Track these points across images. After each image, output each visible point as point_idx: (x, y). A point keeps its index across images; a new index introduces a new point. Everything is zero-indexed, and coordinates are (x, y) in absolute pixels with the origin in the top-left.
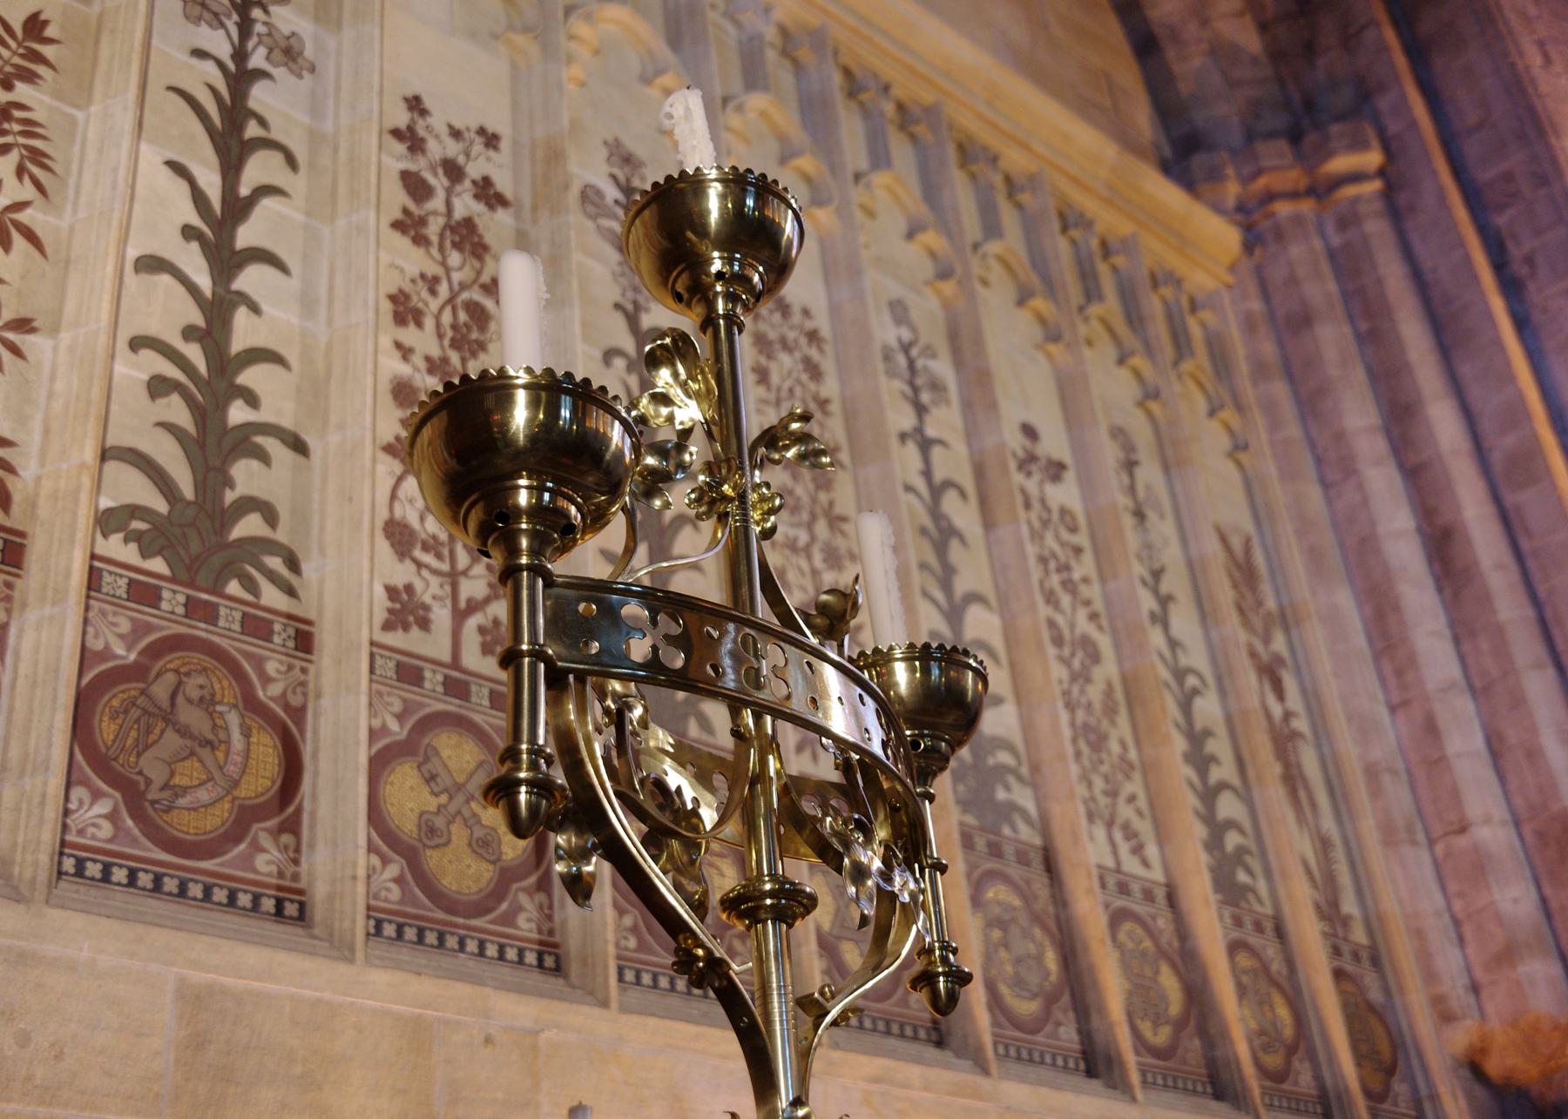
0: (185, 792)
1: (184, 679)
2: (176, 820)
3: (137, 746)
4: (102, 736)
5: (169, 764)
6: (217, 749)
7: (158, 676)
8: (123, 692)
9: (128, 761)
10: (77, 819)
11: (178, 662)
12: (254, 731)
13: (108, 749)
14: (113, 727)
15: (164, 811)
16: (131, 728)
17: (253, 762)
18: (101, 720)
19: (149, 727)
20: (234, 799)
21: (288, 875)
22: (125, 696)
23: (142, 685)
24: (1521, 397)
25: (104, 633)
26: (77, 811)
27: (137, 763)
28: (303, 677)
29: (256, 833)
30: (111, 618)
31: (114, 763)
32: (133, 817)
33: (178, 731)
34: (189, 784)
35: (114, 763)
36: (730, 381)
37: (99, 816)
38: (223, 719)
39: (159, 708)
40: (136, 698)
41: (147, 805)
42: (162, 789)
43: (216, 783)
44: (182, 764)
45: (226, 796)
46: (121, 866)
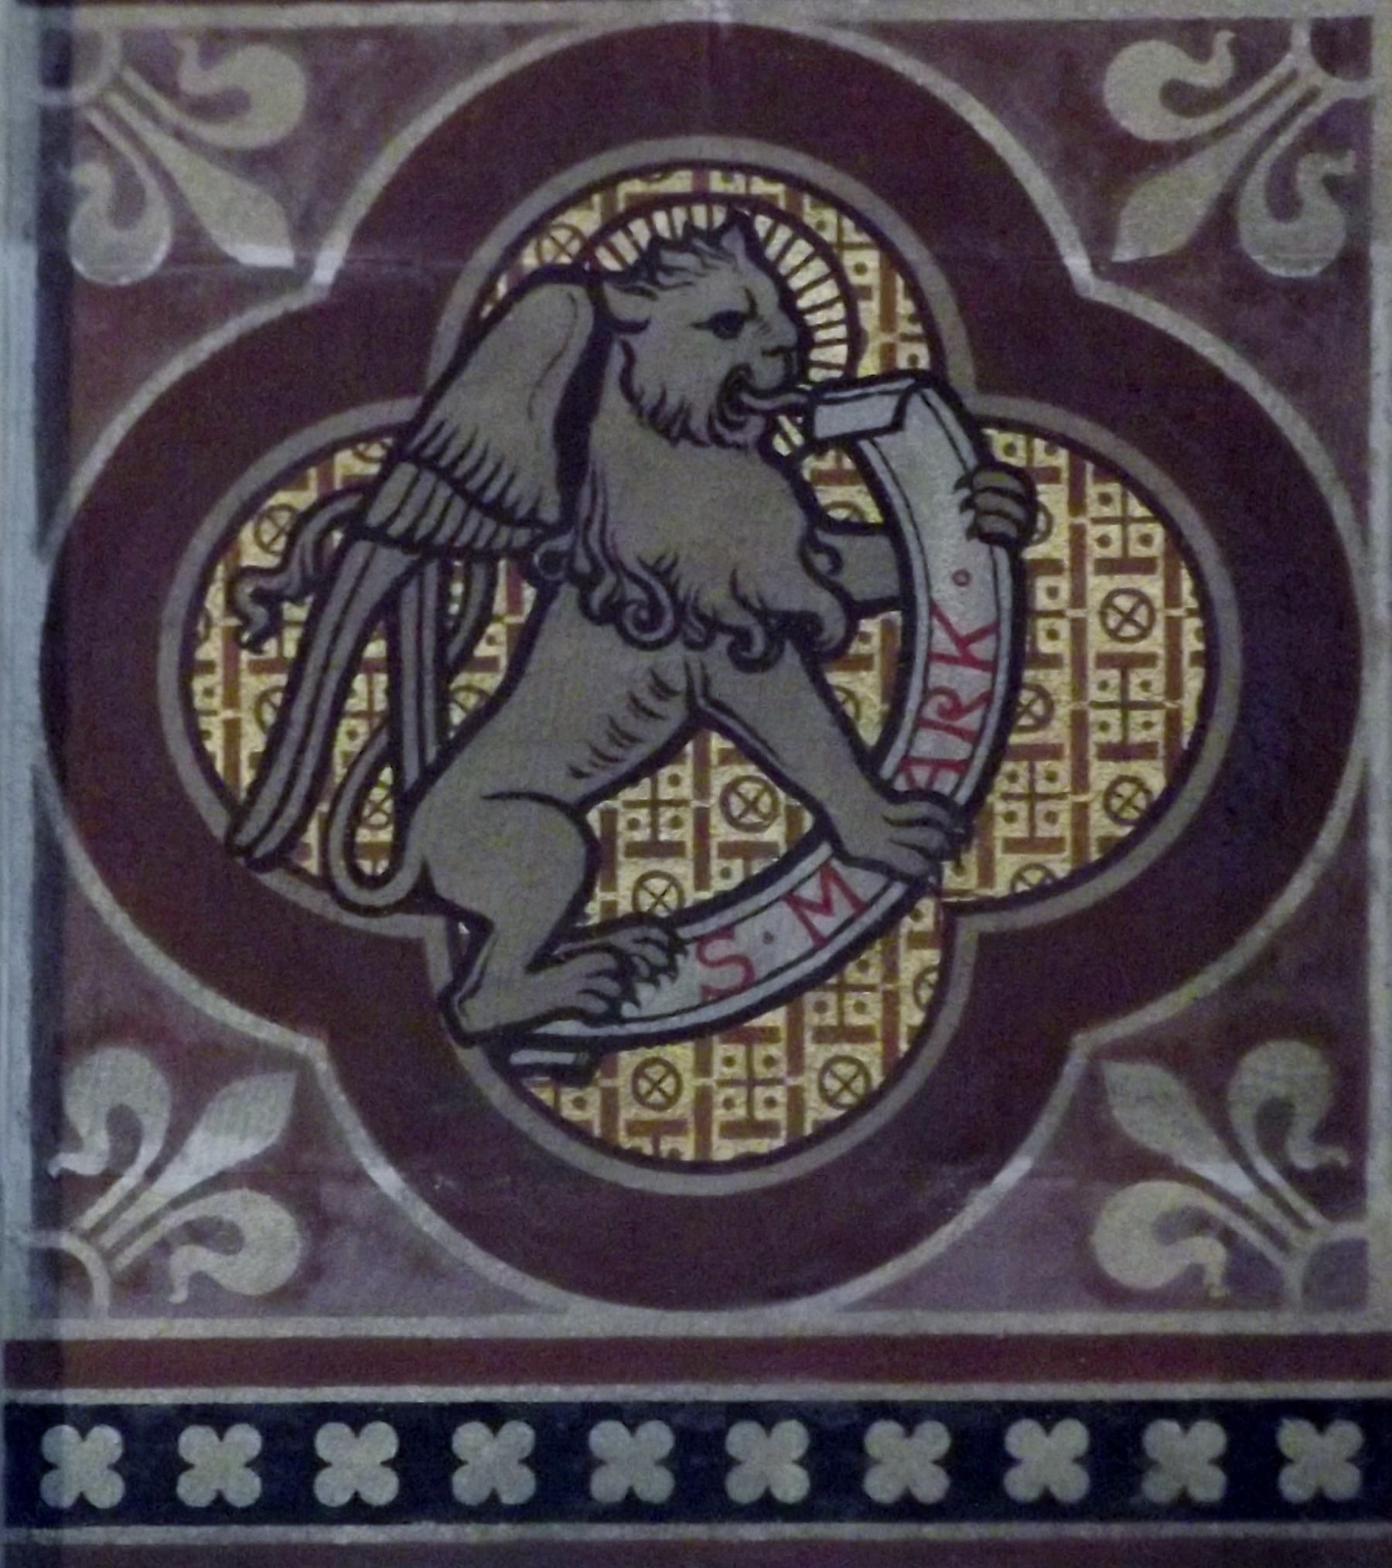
0: (675, 947)
1: (624, 305)
2: (629, 1112)
3: (392, 755)
4: (197, 737)
5: (576, 812)
6: (839, 655)
7: (475, 332)
8: (292, 477)
9: (350, 849)
10: (102, 1226)
11: (587, 220)
12: (1052, 497)
13: (239, 814)
14: (252, 685)
15: (561, 1075)
16: (355, 663)
17: (1057, 681)
18: (189, 667)
19: (443, 637)
20: (953, 912)
21: (1293, 1273)
22: (303, 498)
23: (403, 409)
24: (991, 1307)
25: (167, 180)
26: (107, 1179)
27: (397, 850)
28: (1336, 89)
29: (1092, 1079)
30: (194, 79)
31: (273, 880)
32: (396, 1150)
33: (610, 614)
34: (694, 896)
35: (273, 880)
36: (1256, 98)
37: (220, 1182)
38: (866, 474)
39: (499, 511)
40: (367, 489)
41: (472, 1059)
42: (542, 961)
43: (840, 852)
44: (640, 791)
45: (904, 907)
46: (357, 1417)
